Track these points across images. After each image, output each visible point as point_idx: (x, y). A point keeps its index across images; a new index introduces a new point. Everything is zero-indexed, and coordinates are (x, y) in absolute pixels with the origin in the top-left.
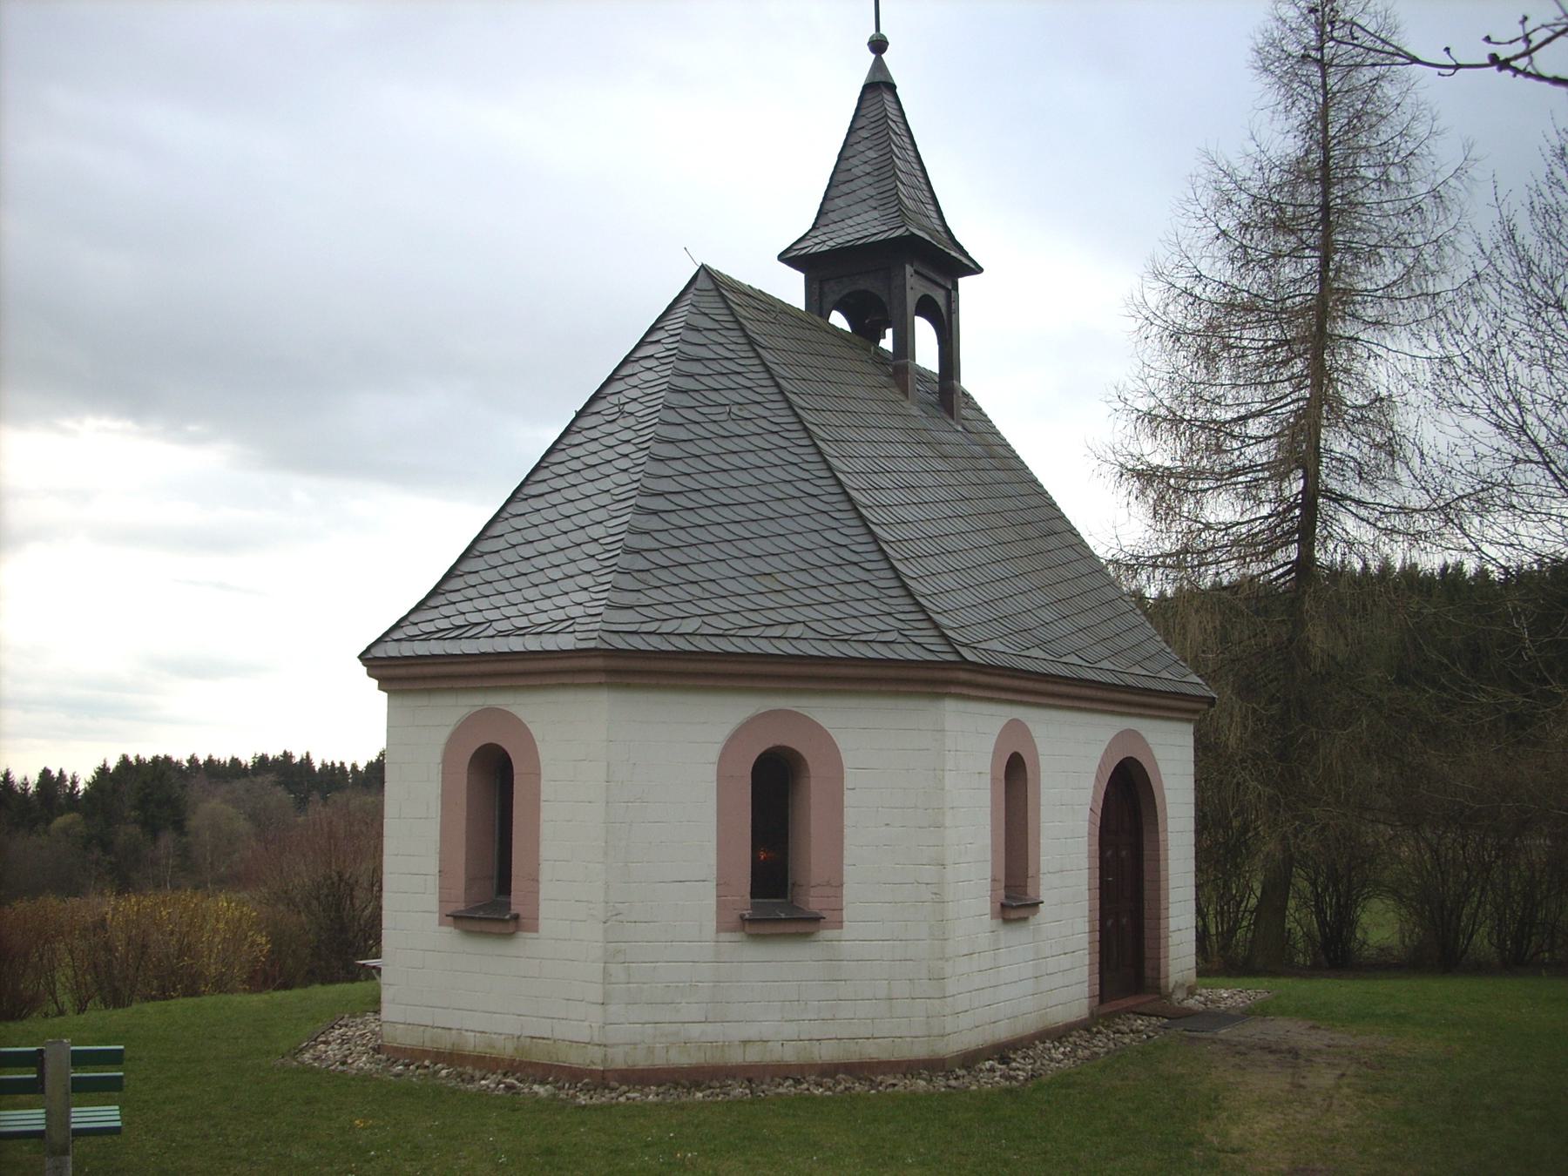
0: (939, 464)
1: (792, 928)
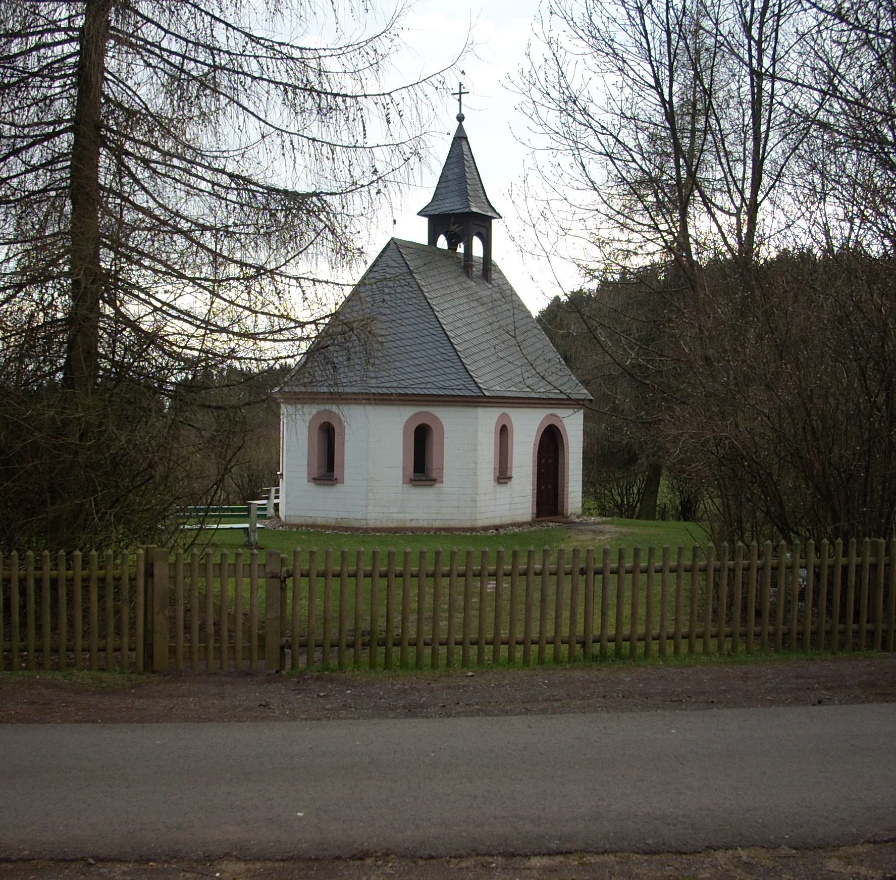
0: (480, 309)
1: (427, 483)
